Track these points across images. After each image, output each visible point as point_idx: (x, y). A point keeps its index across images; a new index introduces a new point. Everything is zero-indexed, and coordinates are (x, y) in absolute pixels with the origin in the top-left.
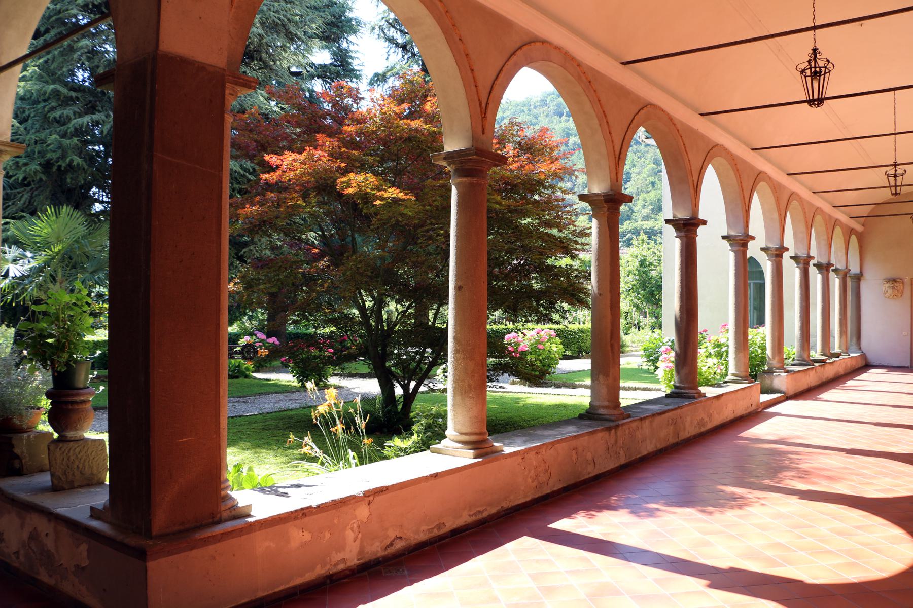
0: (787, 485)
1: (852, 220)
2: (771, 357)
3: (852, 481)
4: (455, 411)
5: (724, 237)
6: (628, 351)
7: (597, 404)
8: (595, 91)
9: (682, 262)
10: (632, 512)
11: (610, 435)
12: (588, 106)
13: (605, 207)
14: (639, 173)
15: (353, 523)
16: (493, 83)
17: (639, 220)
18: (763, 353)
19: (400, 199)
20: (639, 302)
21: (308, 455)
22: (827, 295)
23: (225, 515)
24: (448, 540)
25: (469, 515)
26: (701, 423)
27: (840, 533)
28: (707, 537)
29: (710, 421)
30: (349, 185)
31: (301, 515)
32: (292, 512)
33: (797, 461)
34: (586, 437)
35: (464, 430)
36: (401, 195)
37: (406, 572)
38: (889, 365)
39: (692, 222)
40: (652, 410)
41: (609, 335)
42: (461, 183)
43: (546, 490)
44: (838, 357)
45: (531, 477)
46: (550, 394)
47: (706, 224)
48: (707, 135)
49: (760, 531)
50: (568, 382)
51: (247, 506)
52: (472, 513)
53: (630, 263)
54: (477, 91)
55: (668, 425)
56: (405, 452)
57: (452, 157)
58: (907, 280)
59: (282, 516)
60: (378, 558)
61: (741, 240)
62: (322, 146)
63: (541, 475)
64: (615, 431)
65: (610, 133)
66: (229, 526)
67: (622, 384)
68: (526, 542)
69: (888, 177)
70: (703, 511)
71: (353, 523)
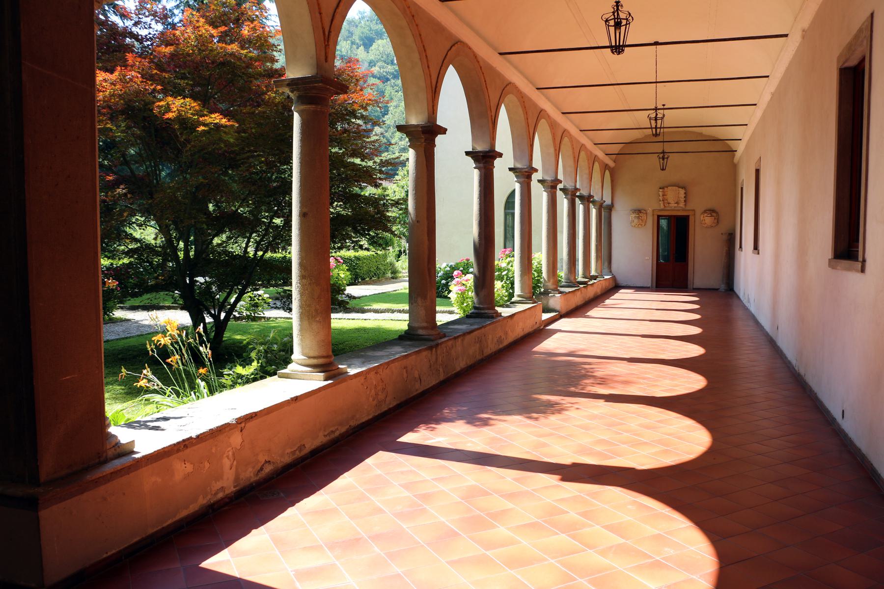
0: (590, 391)
1: (607, 157)
2: (546, 280)
3: (642, 384)
4: (302, 336)
5: (510, 169)
6: (400, 277)
7: (416, 325)
8: (417, 25)
9: (480, 191)
10: (468, 423)
11: (432, 354)
12: (410, 40)
13: (422, 138)
14: (396, 107)
15: (229, 451)
16: (335, 12)
17: (397, 152)
18: (538, 276)
19: (222, 126)
20: (405, 231)
21: (145, 388)
22: (588, 223)
23: (110, 453)
24: (308, 461)
25: (325, 436)
26: (500, 340)
27: (648, 427)
28: (542, 440)
29: (506, 339)
30: (168, 109)
31: (182, 446)
32: (174, 444)
33: (591, 370)
34: (414, 357)
35: (312, 354)
36: (224, 121)
37: (282, 495)
38: (635, 285)
39: (491, 154)
40: (461, 329)
41: (426, 260)
42: (305, 110)
43: (384, 408)
44: (595, 279)
45: (372, 396)
46: (344, 319)
47: (502, 157)
48: (503, 73)
49: (584, 431)
50: (357, 307)
51: (130, 442)
52: (326, 433)
53: (396, 193)
54: (321, 18)
55: (475, 343)
56: (248, 381)
57: (296, 84)
58: (650, 211)
59: (167, 449)
60: (252, 484)
61: (526, 172)
62: (132, 66)
63: (380, 393)
64: (436, 349)
65: (428, 67)
66: (118, 463)
67: (438, 308)
68: (382, 456)
69: (650, 120)
70: (530, 418)
71: (229, 451)
